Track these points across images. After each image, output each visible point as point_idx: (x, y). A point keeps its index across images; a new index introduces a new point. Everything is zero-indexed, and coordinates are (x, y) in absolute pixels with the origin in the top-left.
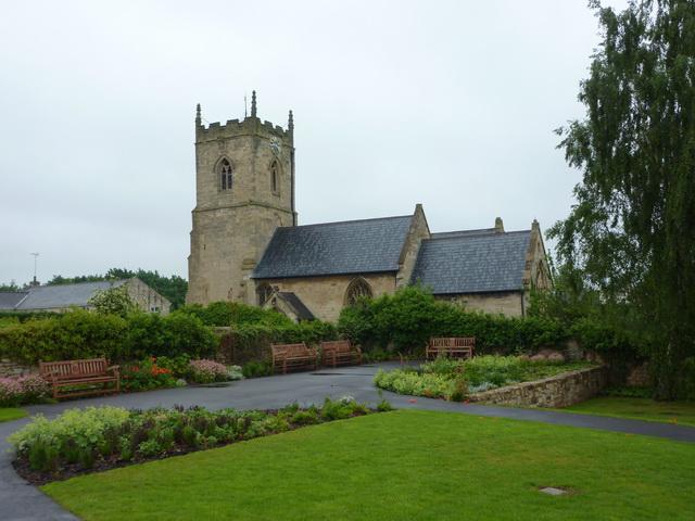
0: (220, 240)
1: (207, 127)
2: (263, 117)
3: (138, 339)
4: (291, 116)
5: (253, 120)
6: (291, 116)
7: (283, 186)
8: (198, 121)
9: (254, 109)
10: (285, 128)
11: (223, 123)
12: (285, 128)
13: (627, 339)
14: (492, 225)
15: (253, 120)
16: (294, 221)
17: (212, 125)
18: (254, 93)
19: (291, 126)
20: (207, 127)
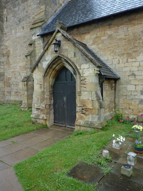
0: (16, 9)
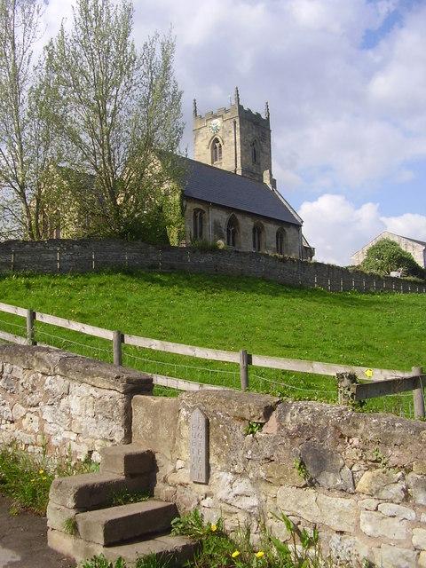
10: (264, 117)
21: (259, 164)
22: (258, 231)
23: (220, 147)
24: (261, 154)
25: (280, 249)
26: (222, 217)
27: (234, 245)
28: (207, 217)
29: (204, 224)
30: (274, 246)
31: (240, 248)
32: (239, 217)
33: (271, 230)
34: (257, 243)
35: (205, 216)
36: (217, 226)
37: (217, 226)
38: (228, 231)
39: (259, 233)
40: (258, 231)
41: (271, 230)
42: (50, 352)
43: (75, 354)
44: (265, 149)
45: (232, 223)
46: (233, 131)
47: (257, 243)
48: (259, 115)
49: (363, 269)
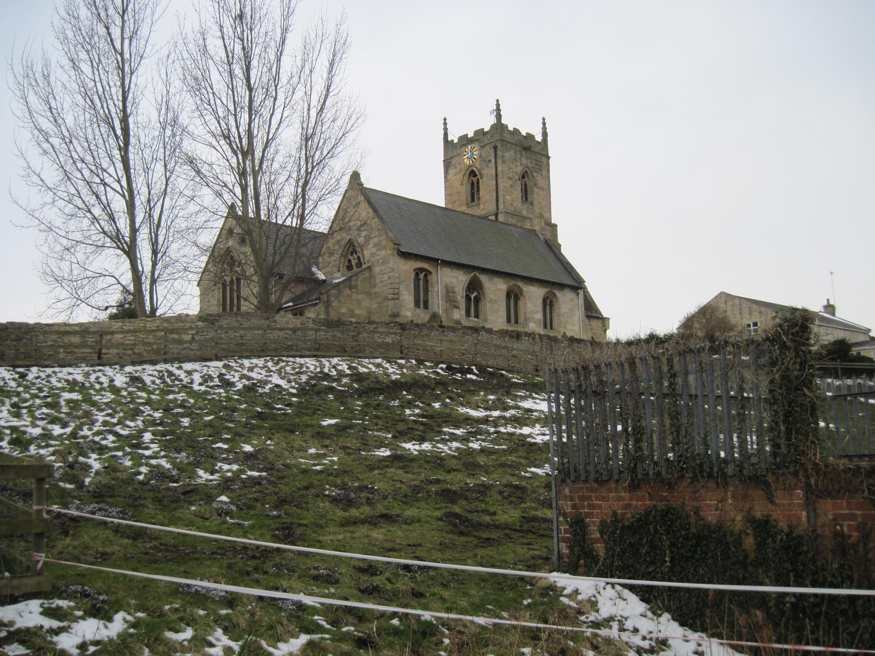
1: (456, 141)
2: (510, 121)
3: (464, 597)
4: (544, 124)
5: (499, 127)
6: (544, 124)
7: (536, 196)
8: (446, 135)
9: (499, 116)
10: (539, 138)
11: (471, 135)
12: (539, 138)
13: (627, 359)
14: (487, 123)
15: (499, 127)
16: (302, 224)
17: (461, 138)
18: (544, 119)
19: (545, 134)
20: (456, 141)
21: (532, 204)
22: (513, 296)
23: (478, 182)
24: (536, 190)
25: (548, 322)
26: (459, 280)
27: (516, 322)
28: (435, 280)
29: (430, 289)
30: (539, 316)
31: (486, 320)
32: (484, 278)
33: (534, 295)
34: (513, 315)
35: (432, 278)
36: (449, 292)
37: (449, 292)
38: (468, 298)
39: (517, 299)
40: (513, 296)
41: (534, 295)
42: (314, 523)
43: (446, 505)
44: (540, 181)
45: (474, 286)
46: (493, 161)
47: (513, 315)
48: (530, 137)
49: (201, 314)
